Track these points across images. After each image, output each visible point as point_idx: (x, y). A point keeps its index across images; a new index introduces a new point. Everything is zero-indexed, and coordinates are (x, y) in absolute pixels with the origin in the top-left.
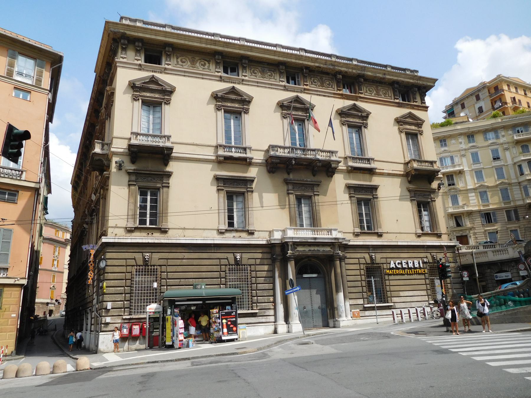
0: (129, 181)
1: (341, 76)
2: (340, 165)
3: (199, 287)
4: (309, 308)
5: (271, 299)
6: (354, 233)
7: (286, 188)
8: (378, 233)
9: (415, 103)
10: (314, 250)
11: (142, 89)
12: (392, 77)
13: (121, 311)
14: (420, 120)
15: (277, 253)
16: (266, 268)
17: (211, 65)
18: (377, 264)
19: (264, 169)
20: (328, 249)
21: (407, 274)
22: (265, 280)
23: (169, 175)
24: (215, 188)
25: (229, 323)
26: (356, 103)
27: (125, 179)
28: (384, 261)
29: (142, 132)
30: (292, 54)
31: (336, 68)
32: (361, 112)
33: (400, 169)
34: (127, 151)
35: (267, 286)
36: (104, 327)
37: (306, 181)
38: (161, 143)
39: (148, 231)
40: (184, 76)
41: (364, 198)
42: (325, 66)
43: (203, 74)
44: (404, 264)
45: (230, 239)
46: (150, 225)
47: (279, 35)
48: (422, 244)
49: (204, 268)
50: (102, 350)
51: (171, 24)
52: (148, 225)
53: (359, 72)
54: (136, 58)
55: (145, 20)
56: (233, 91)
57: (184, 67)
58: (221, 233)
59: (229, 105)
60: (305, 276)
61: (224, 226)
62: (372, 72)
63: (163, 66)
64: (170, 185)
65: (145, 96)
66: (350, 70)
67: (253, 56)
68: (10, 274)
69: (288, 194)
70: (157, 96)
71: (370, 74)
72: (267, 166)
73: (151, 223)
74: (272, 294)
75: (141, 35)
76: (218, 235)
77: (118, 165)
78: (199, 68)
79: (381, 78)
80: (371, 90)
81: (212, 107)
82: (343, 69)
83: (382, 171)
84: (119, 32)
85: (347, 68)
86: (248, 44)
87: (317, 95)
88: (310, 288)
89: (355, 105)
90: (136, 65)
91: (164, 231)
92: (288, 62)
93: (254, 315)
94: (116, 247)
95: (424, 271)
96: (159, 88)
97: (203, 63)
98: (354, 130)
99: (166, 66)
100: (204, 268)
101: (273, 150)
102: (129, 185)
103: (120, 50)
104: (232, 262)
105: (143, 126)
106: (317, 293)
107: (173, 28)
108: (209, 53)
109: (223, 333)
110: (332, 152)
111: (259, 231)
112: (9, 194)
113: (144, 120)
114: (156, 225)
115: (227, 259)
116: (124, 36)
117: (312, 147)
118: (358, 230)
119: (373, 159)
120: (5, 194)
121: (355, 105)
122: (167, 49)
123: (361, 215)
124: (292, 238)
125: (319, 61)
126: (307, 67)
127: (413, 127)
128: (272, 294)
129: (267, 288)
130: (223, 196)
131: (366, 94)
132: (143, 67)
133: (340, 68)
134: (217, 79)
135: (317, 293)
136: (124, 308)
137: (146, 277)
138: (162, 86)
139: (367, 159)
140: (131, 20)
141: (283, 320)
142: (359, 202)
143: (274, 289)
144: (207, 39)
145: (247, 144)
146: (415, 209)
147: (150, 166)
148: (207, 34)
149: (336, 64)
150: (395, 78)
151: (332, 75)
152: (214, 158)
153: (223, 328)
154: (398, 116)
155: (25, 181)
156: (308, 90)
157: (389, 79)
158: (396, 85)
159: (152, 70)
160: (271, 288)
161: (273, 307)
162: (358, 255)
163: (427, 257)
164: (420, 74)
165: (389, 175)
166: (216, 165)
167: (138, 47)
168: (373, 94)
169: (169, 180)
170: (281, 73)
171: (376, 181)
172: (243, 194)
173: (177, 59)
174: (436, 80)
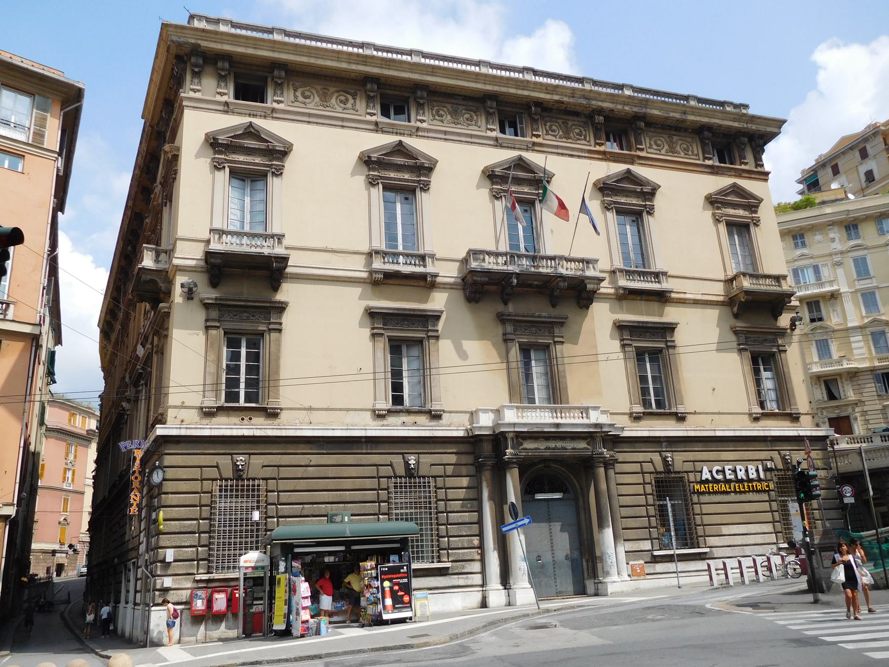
0: (207, 320)
1: (601, 118)
3: (338, 519)
4: (547, 557)
5: (476, 541)
7: (500, 330)
9: (743, 167)
11: (503, 179)
12: (698, 119)
13: (192, 566)
14: (647, 183)
15: (485, 453)
16: (465, 482)
17: (358, 101)
18: (676, 472)
19: (459, 295)
20: (582, 445)
21: (735, 492)
22: (462, 506)
23: (281, 308)
25: (396, 588)
27: (200, 315)
28: (689, 467)
29: (231, 228)
30: (509, 79)
31: (593, 102)
32: (641, 185)
33: (717, 291)
38: (266, 249)
40: (309, 122)
41: (650, 347)
42: (571, 100)
43: (343, 119)
44: (728, 472)
48: (761, 434)
49: (348, 484)
52: (242, 402)
53: (635, 109)
56: (400, 149)
57: (308, 106)
58: (379, 416)
59: (392, 175)
60: (539, 496)
61: (385, 404)
62: (661, 109)
63: (269, 104)
64: (283, 326)
66: (620, 107)
70: (407, 176)
72: (464, 289)
76: (374, 420)
77: (186, 290)
78: (335, 108)
79: (678, 120)
80: (659, 142)
82: (606, 105)
83: (682, 296)
85: (613, 103)
87: (558, 154)
88: (549, 520)
89: (629, 171)
91: (272, 414)
94: (182, 445)
96: (263, 146)
97: (343, 98)
100: (348, 484)
103: (188, 77)
106: (562, 530)
107: (287, 34)
109: (384, 607)
110: (587, 262)
111: (451, 412)
113: (234, 205)
114: (257, 402)
115: (391, 465)
116: (196, 50)
117: (550, 252)
118: (639, 409)
123: (643, 379)
125: (560, 90)
126: (539, 103)
127: (741, 212)
128: (477, 533)
129: (467, 520)
130: (382, 346)
131: (649, 150)
132: (231, 107)
133: (600, 103)
135: (562, 530)
138: (267, 141)
139: (653, 273)
140: (208, 20)
141: (499, 581)
142: (640, 354)
143: (480, 522)
145: (658, 265)
146: (748, 368)
147: (246, 291)
148: (350, 44)
149: (592, 95)
150: (705, 120)
153: (384, 597)
155: (13, 321)
156: (541, 145)
157: (693, 122)
158: (706, 133)
159: (248, 112)
160: (475, 520)
161: (478, 557)
162: (640, 457)
163: (772, 460)
164: (751, 111)
165: (696, 303)
166: (369, 288)
167: (223, 70)
168: (663, 152)
169: (280, 318)
171: (671, 314)
172: (420, 342)
173: (295, 90)
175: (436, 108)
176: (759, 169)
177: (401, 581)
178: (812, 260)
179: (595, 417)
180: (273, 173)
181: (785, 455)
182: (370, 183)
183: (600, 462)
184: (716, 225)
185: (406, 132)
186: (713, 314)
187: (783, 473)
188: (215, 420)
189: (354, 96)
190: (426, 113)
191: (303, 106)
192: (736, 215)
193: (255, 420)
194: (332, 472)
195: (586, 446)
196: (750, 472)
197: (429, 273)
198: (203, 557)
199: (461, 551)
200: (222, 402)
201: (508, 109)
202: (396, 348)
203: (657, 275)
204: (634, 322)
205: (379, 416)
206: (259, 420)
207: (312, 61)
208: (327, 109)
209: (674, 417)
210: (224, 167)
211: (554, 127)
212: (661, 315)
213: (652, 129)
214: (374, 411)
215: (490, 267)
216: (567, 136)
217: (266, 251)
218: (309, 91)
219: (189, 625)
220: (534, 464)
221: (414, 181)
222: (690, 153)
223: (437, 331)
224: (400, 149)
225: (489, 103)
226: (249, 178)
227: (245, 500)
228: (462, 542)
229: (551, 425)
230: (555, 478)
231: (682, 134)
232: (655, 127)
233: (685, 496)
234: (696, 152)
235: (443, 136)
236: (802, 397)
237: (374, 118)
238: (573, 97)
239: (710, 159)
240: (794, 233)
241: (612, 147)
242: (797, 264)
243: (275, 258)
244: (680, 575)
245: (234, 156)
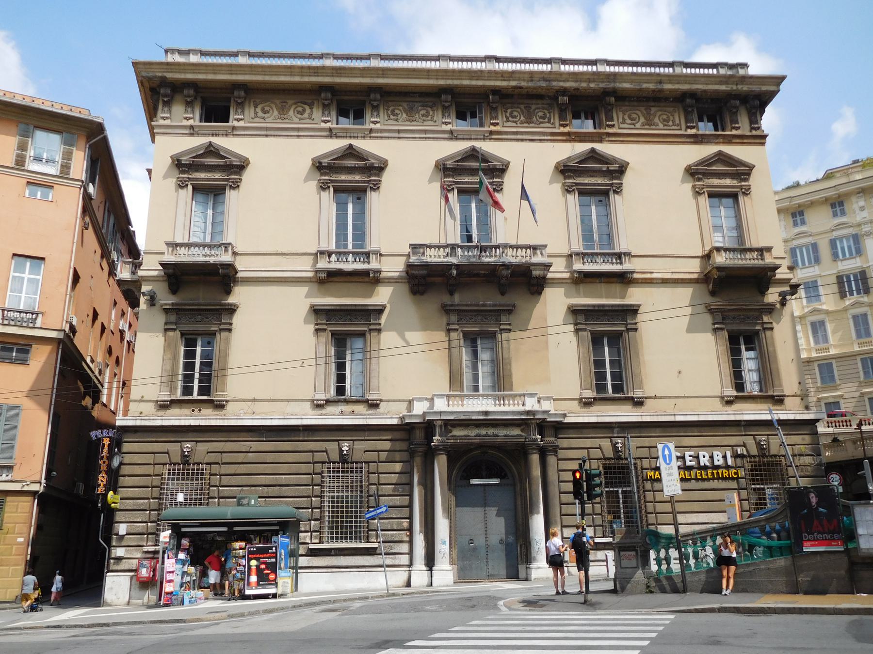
0: (166, 324)
1: (566, 98)
3: (245, 501)
4: (480, 541)
5: (405, 524)
6: (581, 399)
7: (444, 320)
8: (633, 398)
9: (734, 132)
10: (487, 435)
11: (192, 167)
12: (677, 86)
13: (142, 539)
14: (614, 160)
15: (416, 439)
16: (398, 467)
17: (314, 110)
18: (771, 456)
19: (404, 288)
20: (516, 432)
21: (697, 479)
22: (394, 490)
23: (232, 310)
24: (311, 328)
25: (263, 566)
27: (160, 319)
28: (644, 452)
29: (194, 240)
30: (461, 71)
31: (554, 84)
32: (607, 164)
33: (694, 267)
34: (404, 274)
35: (397, 500)
36: (114, 564)
37: (483, 305)
38: (750, 260)
39: (192, 406)
40: (266, 136)
41: (608, 332)
42: (530, 84)
43: (298, 129)
44: (688, 459)
45: (334, 417)
47: (556, 40)
48: (732, 418)
49: (284, 468)
50: (109, 601)
51: (331, 51)
52: (195, 396)
53: (602, 85)
55: (203, 49)
56: (350, 152)
58: (318, 406)
59: (343, 177)
62: (632, 82)
63: (233, 123)
64: (234, 326)
65: (197, 179)
66: (584, 85)
67: (387, 85)
68: (14, 475)
69: (449, 331)
70: (357, 178)
71: (626, 85)
72: (409, 282)
73: (614, 391)
74: (407, 516)
75: (190, 76)
76: (313, 409)
77: (149, 298)
78: (294, 119)
79: (653, 91)
80: (634, 116)
81: (557, 187)
82: (568, 85)
83: (648, 276)
84: (155, 77)
85: (576, 81)
87: (518, 140)
88: (485, 504)
90: (185, 127)
91: (219, 406)
92: (457, 87)
93: (371, 552)
94: (139, 434)
95: (736, 473)
96: (221, 162)
97: (300, 109)
98: (592, 200)
99: (372, 126)
100: (284, 468)
101: (415, 254)
102: (166, 330)
103: (160, 107)
104: (335, 457)
105: (196, 229)
106: (498, 515)
107: (383, 58)
108: (310, 91)
109: (249, 583)
110: (534, 248)
111: (388, 401)
112: (18, 351)
113: (197, 219)
114: (209, 395)
115: (600, 448)
116: (164, 82)
117: (501, 240)
118: (590, 394)
119: (628, 254)
120: (11, 350)
122: (372, 96)
123: (599, 364)
124: (440, 413)
125: (517, 75)
126: (496, 91)
127: (728, 182)
128: (407, 516)
129: (398, 504)
130: (324, 340)
131: (622, 126)
132: (196, 130)
133: (562, 84)
134: (446, 136)
135: (498, 515)
136: (312, 532)
137: (185, 482)
139: (615, 254)
140: (181, 52)
141: (423, 562)
142: (597, 340)
143: (410, 506)
144: (302, 67)
145: (622, 246)
146: (724, 346)
147: (199, 296)
148: (311, 56)
149: (552, 76)
151: (550, 98)
152: (310, 275)
153: (249, 575)
155: (41, 328)
156: (499, 133)
157: (671, 90)
158: (688, 101)
159: (211, 132)
160: (406, 503)
161: (407, 539)
162: (588, 443)
163: (744, 445)
164: (752, 71)
165: (665, 282)
166: (315, 286)
167: (189, 96)
168: (638, 125)
169: (231, 318)
170: (445, 109)
171: (634, 296)
172: (362, 335)
173: (256, 107)
174: (782, 78)
175: (391, 109)
176: (754, 133)
177: (269, 560)
178: (851, 229)
179: (531, 404)
180: (231, 186)
181: (760, 441)
182: (567, 190)
183: (534, 449)
184: (696, 198)
185: (360, 135)
186: (685, 293)
187: (612, 462)
188: (169, 412)
189: (311, 106)
191: (262, 120)
192: (722, 183)
193: (204, 411)
194: (270, 457)
195: (520, 433)
196: (716, 458)
197: (371, 270)
198: (152, 531)
199: (390, 533)
200: (178, 395)
201: (466, 100)
202: (340, 341)
203: (619, 256)
204: (589, 306)
205: (318, 406)
206: (208, 411)
207: (267, 78)
208: (285, 121)
209: (631, 402)
210: (187, 185)
213: (627, 103)
214: (722, 398)
215: (429, 260)
217: (212, 260)
218: (268, 106)
219: (137, 590)
220: (471, 450)
221: (364, 182)
222: (671, 123)
223: (380, 324)
224: (350, 152)
225: (443, 97)
226: (211, 193)
227: (190, 482)
228: (392, 524)
229: (479, 413)
230: (489, 466)
231: (662, 104)
232: (630, 101)
233: (783, 479)
234: (677, 122)
235: (397, 135)
236: (789, 380)
237: (328, 125)
238: (532, 81)
240: (832, 202)
241: (706, 128)
242: (836, 234)
243: (221, 265)
244: (387, 569)
245: (196, 174)
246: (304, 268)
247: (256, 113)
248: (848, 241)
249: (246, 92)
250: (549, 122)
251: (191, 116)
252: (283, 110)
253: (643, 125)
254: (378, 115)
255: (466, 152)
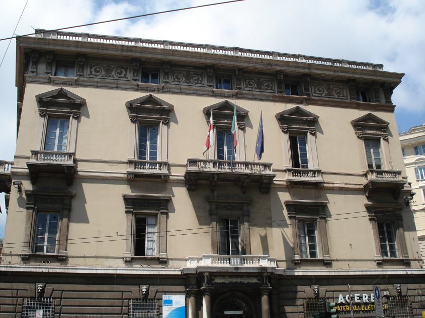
2: (405, 186)
17: (128, 73)
26: (302, 107)
44: (356, 298)
45: (138, 269)
46: (311, 257)
49: (104, 302)
52: (45, 253)
54: (208, 84)
56: (150, 100)
57: (98, 77)
60: (227, 313)
61: (130, 255)
70: (375, 132)
80: (321, 89)
83: (331, 185)
86: (62, 38)
89: (298, 108)
97: (119, 71)
100: (104, 302)
103: (31, 65)
116: (34, 51)
121: (298, 108)
126: (241, 70)
138: (70, 98)
148: (129, 40)
150: (351, 75)
154: (354, 119)
167: (49, 59)
168: (323, 95)
173: (91, 68)
176: (388, 104)
183: (265, 292)
189: (126, 70)
190: (170, 78)
192: (371, 133)
206: (57, 265)
208: (109, 78)
211: (251, 83)
212: (317, 198)
216: (259, 87)
218: (98, 68)
222: (342, 95)
234: (345, 95)
239: (354, 99)
243: (66, 167)
246: (123, 170)
247: (91, 72)
248: (421, 170)
249: (170, 66)
250: (271, 89)
251: (35, 70)
252: (108, 71)
253: (326, 95)
254: (168, 78)
255: (223, 104)
